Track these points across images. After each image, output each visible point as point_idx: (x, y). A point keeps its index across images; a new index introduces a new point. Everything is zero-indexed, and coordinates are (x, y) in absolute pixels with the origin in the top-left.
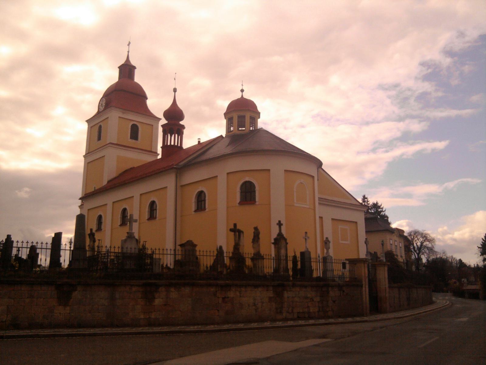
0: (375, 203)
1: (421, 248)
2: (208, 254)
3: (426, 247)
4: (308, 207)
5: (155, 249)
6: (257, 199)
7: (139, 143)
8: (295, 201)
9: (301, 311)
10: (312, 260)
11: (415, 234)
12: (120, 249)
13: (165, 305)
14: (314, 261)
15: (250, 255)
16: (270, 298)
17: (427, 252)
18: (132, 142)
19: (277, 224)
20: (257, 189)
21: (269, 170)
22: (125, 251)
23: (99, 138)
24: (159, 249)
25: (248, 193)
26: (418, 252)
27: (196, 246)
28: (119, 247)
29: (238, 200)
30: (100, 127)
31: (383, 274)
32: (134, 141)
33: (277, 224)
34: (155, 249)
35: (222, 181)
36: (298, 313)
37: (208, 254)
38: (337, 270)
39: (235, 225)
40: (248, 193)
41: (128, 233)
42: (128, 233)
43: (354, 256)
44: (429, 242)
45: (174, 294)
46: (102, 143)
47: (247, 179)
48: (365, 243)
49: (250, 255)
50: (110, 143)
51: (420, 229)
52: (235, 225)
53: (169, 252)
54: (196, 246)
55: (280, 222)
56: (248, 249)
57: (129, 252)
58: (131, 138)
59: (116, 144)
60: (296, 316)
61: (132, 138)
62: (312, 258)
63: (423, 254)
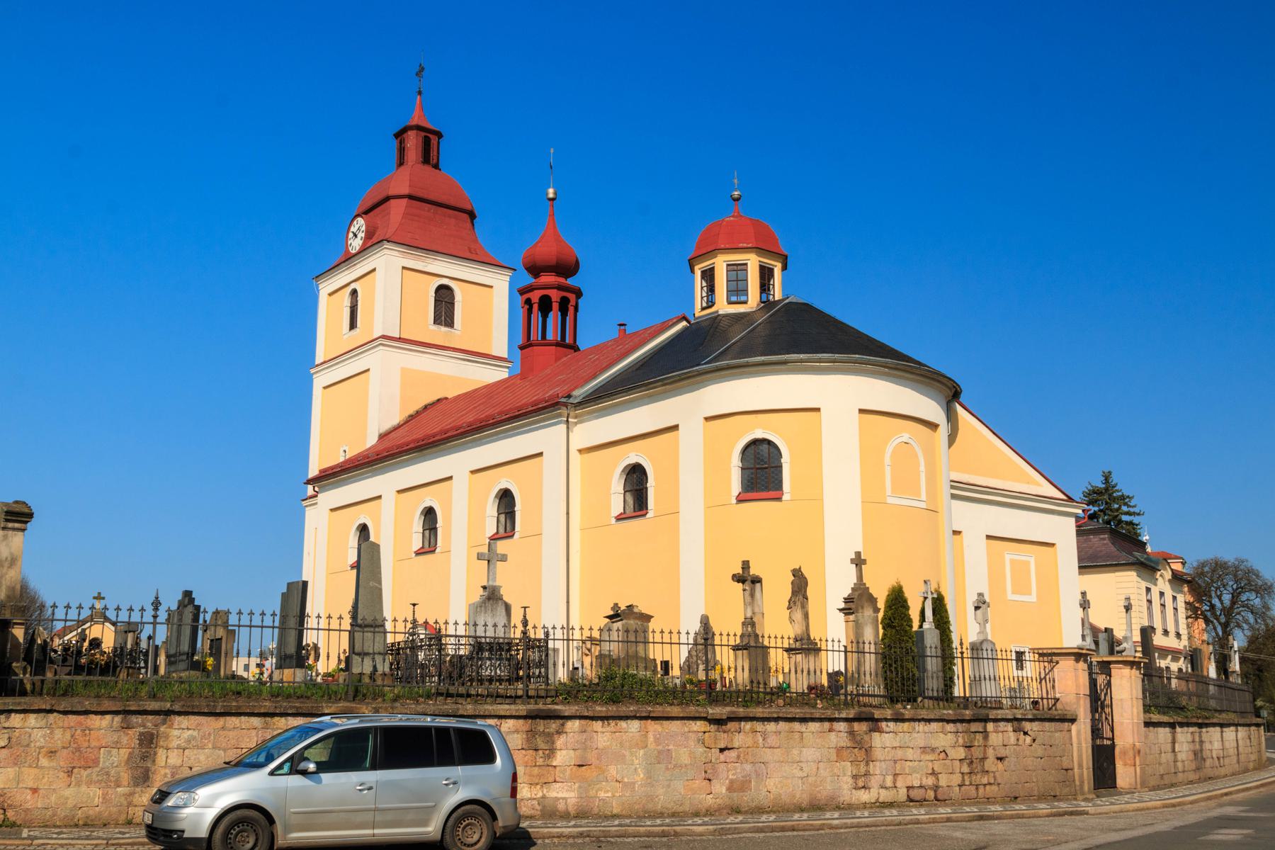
0: (1100, 485)
1: (1232, 607)
2: (257, 620)
3: (1247, 606)
4: (923, 505)
5: (554, 628)
6: (786, 485)
7: (459, 334)
8: (889, 492)
9: (917, 783)
10: (717, 641)
11: (1213, 571)
12: (277, 619)
13: (580, 766)
14: (779, 645)
15: (732, 638)
16: (839, 750)
17: (1252, 620)
18: (439, 334)
19: (852, 561)
20: (786, 460)
21: (818, 410)
22: (480, 632)
23: (353, 325)
24: (662, 632)
25: (762, 471)
26: (1223, 619)
27: (648, 618)
28: (274, 615)
29: (736, 487)
30: (354, 292)
31: (1126, 688)
32: (444, 329)
33: (852, 561)
34: (554, 628)
35: (692, 437)
36: (908, 788)
37: (323, 624)
38: (741, 687)
39: (746, 565)
40: (762, 471)
41: (484, 588)
42: (484, 588)
43: (1048, 643)
44: (1257, 592)
45: (602, 735)
46: (359, 335)
47: (759, 434)
48: (1081, 605)
49: (732, 638)
50: (384, 337)
51: (1229, 557)
52: (746, 565)
53: (684, 640)
54: (648, 618)
55: (858, 554)
56: (778, 627)
57: (490, 633)
58: (435, 322)
59: (400, 339)
60: (902, 795)
61: (437, 321)
62: (717, 633)
63: (1239, 626)
